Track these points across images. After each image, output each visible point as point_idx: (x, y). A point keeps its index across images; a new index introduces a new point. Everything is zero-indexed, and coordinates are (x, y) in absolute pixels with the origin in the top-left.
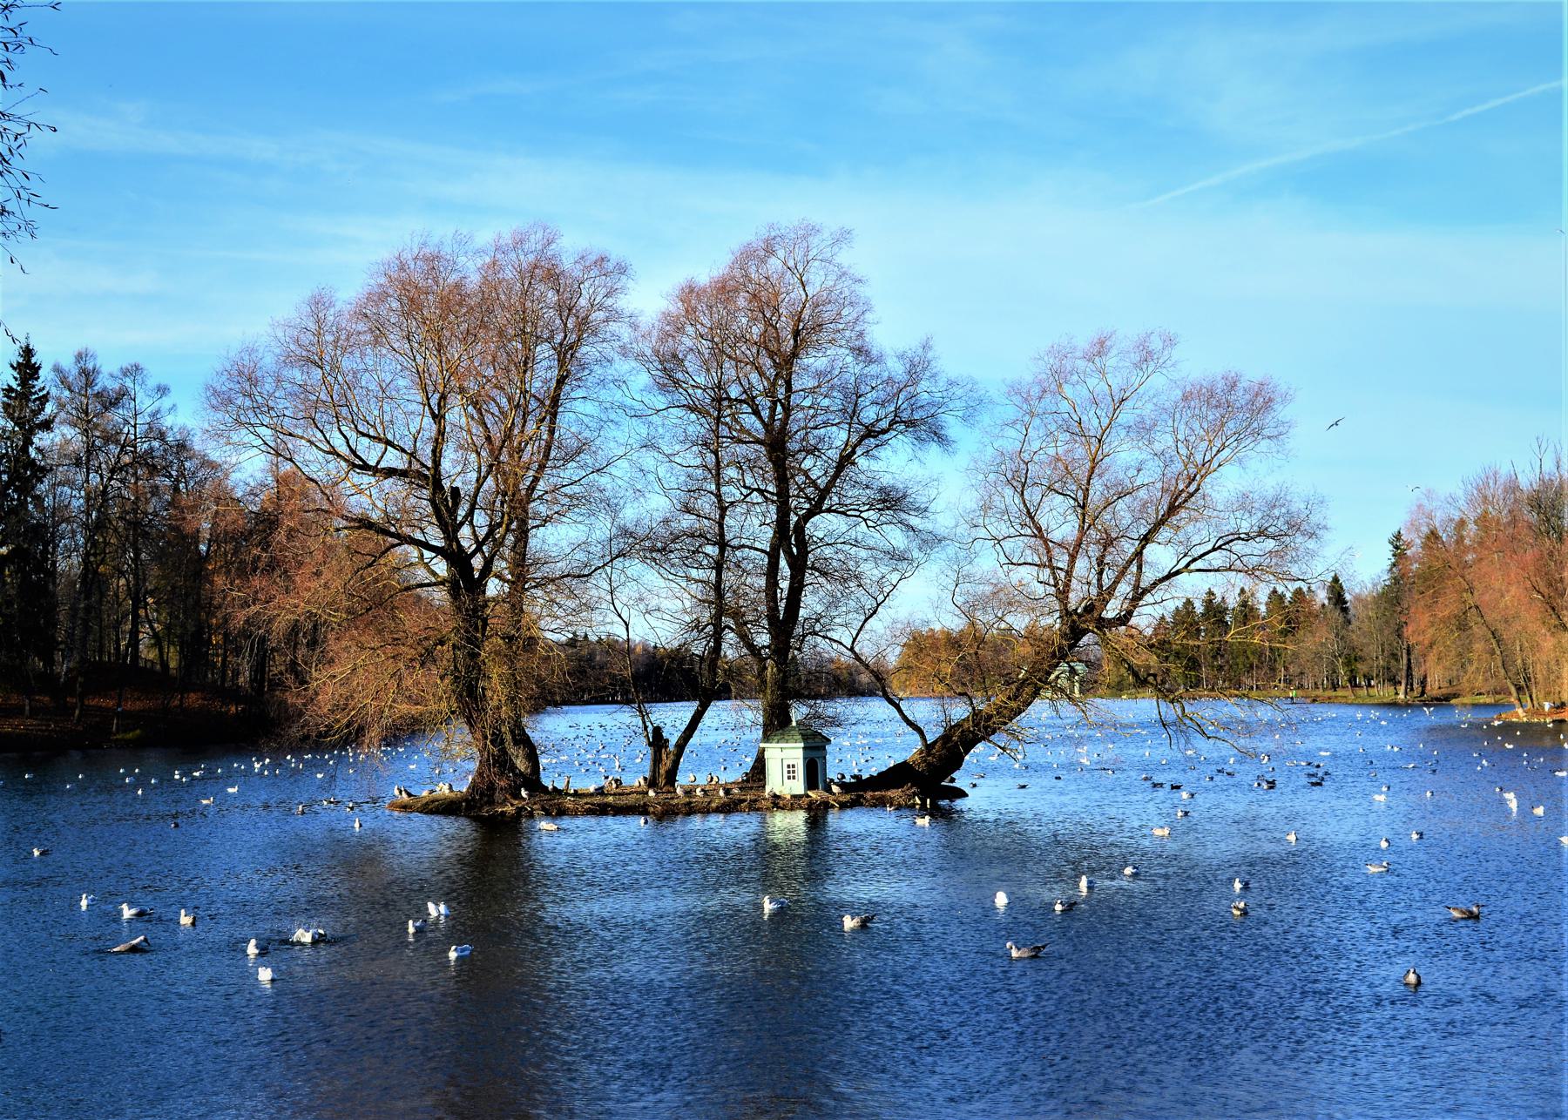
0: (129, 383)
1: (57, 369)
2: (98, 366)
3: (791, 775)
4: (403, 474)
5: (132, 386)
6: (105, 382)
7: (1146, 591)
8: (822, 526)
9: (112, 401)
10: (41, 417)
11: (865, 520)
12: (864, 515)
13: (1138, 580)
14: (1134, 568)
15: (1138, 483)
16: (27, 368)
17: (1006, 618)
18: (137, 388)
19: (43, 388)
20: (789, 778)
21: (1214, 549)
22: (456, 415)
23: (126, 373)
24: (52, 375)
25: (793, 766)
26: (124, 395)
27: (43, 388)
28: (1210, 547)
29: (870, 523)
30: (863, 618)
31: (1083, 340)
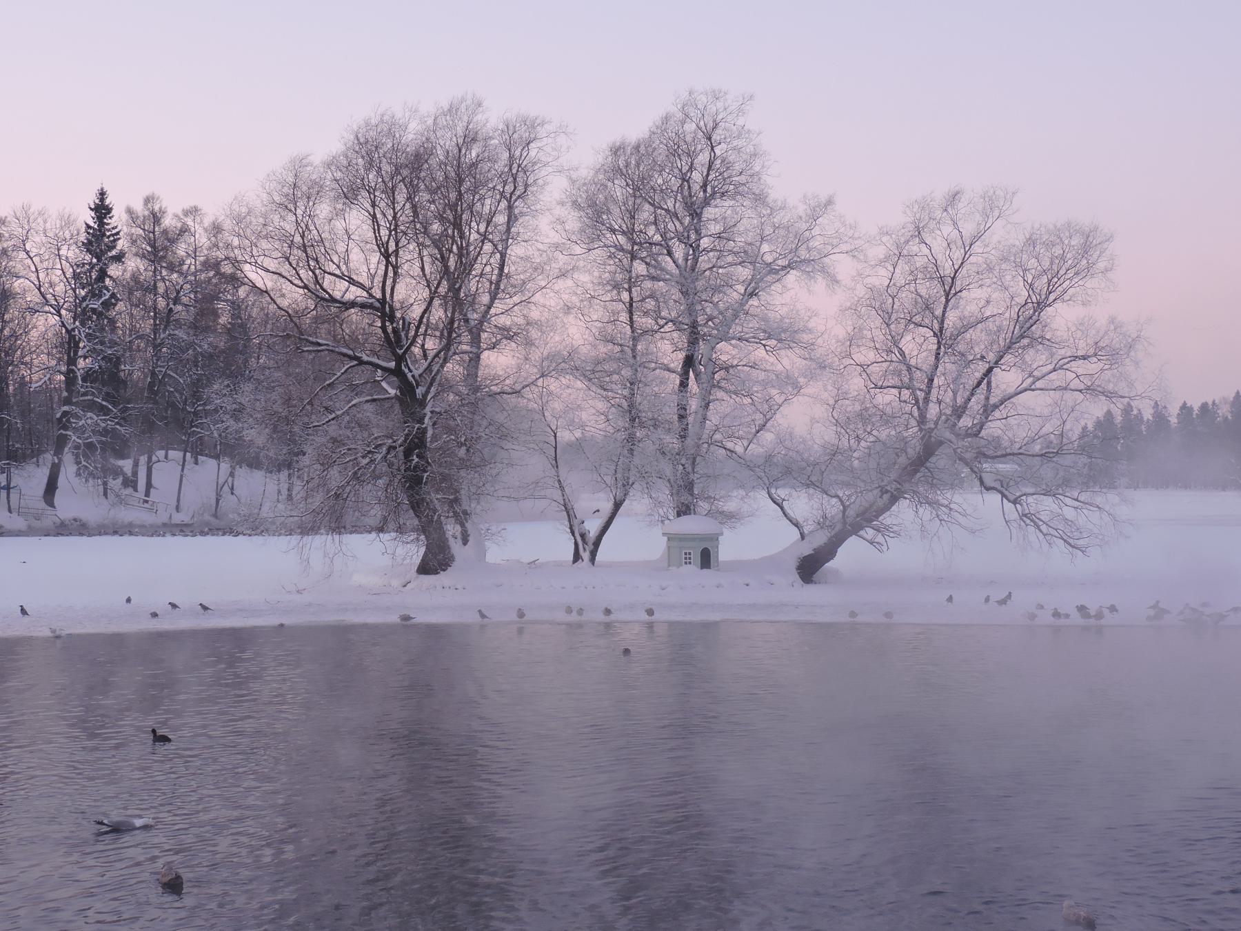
0: (190, 222)
1: (130, 211)
2: (163, 207)
3: (688, 556)
4: (363, 306)
5: (192, 224)
6: (168, 222)
7: (996, 407)
8: (726, 352)
9: (172, 238)
10: (114, 253)
11: (764, 346)
12: (763, 342)
13: (987, 398)
14: (984, 385)
15: (988, 314)
16: (102, 210)
17: (874, 432)
18: (197, 227)
19: (116, 227)
20: (686, 563)
21: (1054, 370)
22: (409, 256)
23: (187, 213)
24: (125, 217)
25: (690, 554)
26: (185, 232)
27: (116, 227)
28: (1050, 367)
29: (768, 348)
30: (754, 431)
31: (940, 192)
